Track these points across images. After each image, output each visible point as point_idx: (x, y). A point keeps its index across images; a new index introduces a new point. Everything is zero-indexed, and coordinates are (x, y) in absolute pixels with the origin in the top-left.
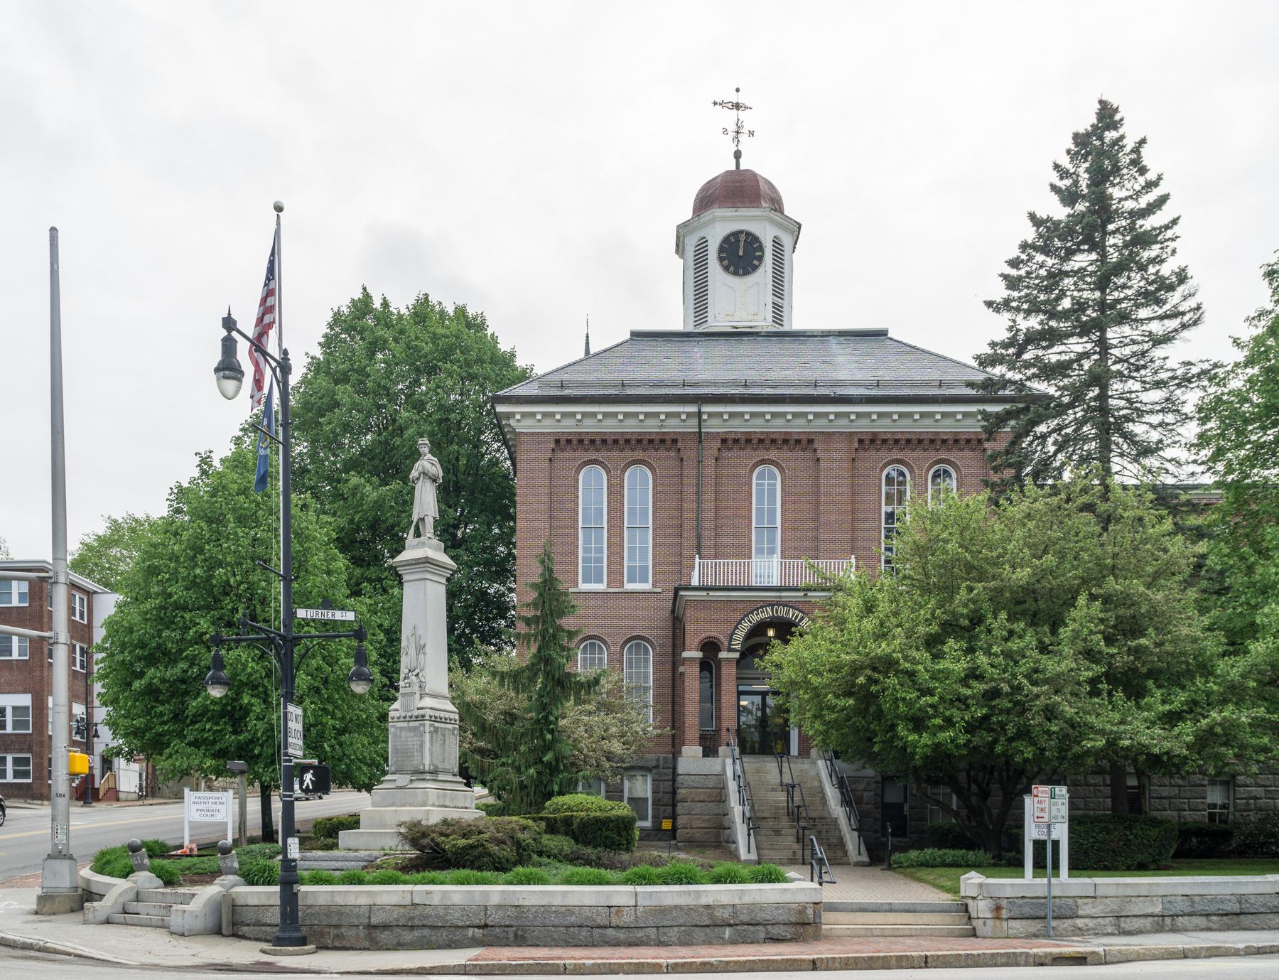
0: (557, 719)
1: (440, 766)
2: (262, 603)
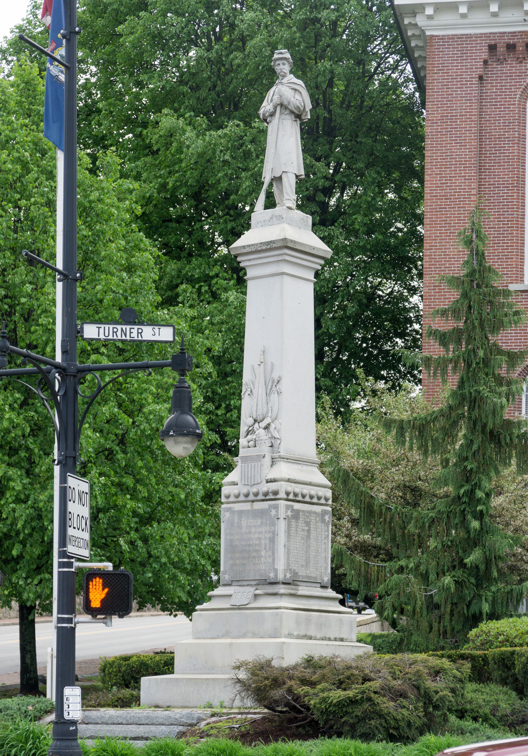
0: (488, 495)
1: (302, 573)
2: (26, 320)
